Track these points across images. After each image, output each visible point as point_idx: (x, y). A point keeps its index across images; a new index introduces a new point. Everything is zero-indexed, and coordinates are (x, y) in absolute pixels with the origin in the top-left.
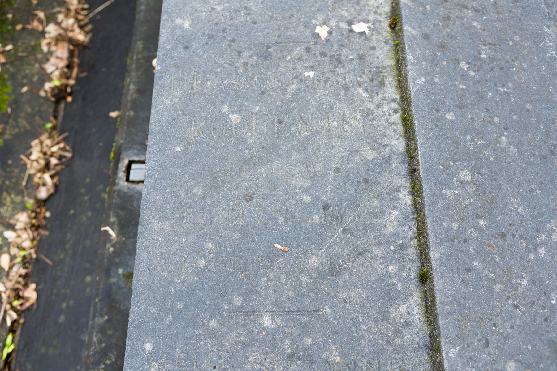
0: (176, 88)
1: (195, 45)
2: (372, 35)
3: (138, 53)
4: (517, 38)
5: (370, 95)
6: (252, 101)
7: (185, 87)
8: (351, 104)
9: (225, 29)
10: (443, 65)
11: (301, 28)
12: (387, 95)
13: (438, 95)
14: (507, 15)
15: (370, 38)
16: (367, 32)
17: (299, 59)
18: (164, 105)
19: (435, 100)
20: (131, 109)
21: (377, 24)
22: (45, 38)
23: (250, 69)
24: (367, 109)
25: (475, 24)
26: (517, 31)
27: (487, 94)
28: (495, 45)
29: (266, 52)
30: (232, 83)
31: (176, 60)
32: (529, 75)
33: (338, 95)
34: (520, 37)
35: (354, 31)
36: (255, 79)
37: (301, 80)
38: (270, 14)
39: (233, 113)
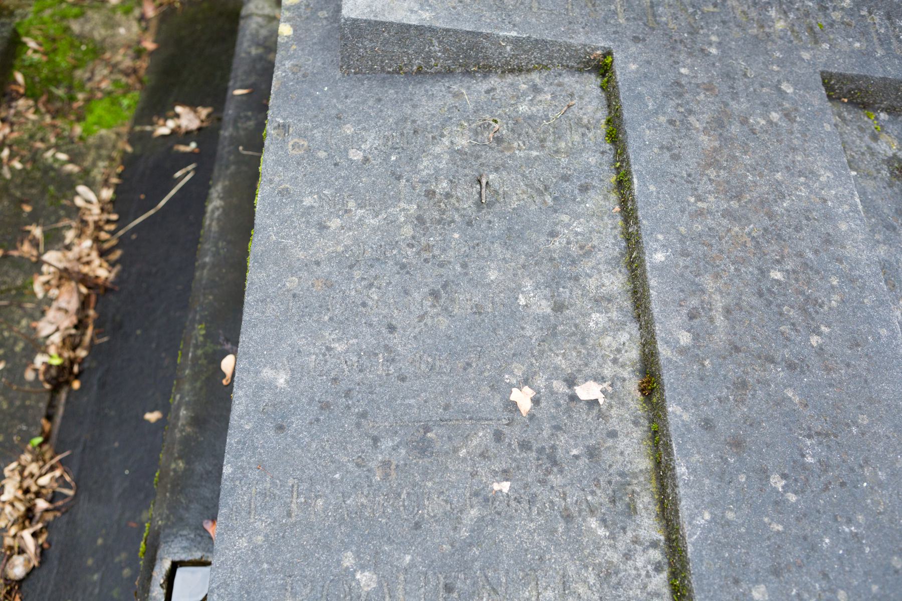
0: (259, 515)
1: (296, 423)
2: (610, 406)
3: (196, 347)
4: (863, 420)
5: (611, 533)
6: (397, 544)
7: (276, 511)
8: (577, 551)
9: (350, 390)
10: (740, 483)
11: (485, 390)
12: (642, 532)
13: (736, 548)
14: (843, 372)
15: (607, 414)
16: (601, 401)
17: (483, 455)
18: (236, 550)
19: (731, 559)
20: (180, 458)
21: (619, 384)
22: (41, 273)
23: (394, 475)
24: (607, 562)
25: (790, 393)
26: (863, 404)
27: (822, 541)
28: (827, 435)
29: (423, 439)
30: (362, 505)
31: (260, 454)
32: (891, 496)
33: (554, 531)
34: (869, 416)
35: (578, 398)
36: (404, 496)
37: (486, 500)
38: (430, 360)
39: (363, 568)
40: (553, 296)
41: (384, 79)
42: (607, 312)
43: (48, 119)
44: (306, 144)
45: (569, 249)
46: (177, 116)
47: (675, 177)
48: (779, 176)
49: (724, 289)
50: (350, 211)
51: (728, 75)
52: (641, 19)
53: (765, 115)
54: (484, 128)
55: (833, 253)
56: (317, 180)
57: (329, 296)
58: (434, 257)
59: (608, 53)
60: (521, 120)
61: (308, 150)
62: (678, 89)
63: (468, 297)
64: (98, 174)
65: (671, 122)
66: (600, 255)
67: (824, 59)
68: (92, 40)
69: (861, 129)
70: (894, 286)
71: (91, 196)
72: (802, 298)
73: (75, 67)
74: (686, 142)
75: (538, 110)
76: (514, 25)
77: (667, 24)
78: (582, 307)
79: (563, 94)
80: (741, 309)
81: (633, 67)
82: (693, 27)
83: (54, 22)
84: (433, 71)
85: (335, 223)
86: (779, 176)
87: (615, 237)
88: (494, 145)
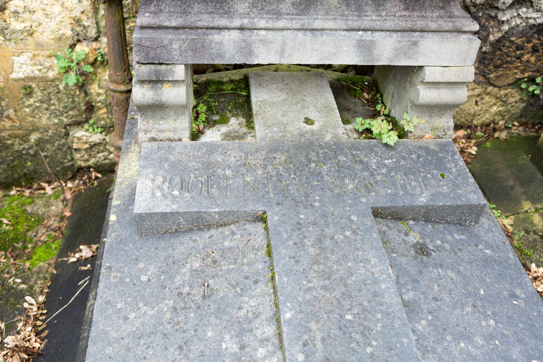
40: (239, 342)
41: (159, 237)
42: (266, 347)
43: (12, 261)
44: (120, 275)
45: (248, 315)
46: (81, 251)
47: (297, 271)
48: (350, 264)
49: (321, 328)
50: (140, 308)
51: (324, 216)
52: (281, 193)
53: (343, 234)
54: (208, 256)
55: (378, 301)
56: (125, 294)
57: (127, 355)
58: (181, 328)
59: (265, 213)
60: (225, 250)
61: (121, 279)
62: (299, 226)
63: (197, 347)
64: (37, 289)
65: (295, 244)
66: (263, 317)
67: (372, 201)
68: (38, 215)
69: (399, 231)
70: (418, 313)
71: (33, 301)
72: (362, 328)
73: (28, 231)
74: (302, 253)
75: (234, 244)
76: (218, 205)
77: (294, 194)
78: (254, 346)
79: (246, 234)
80: (330, 338)
81: (276, 218)
82: (307, 193)
83: (18, 208)
84: (183, 230)
85: (132, 316)
86: (350, 264)
87: (271, 306)
88: (212, 264)
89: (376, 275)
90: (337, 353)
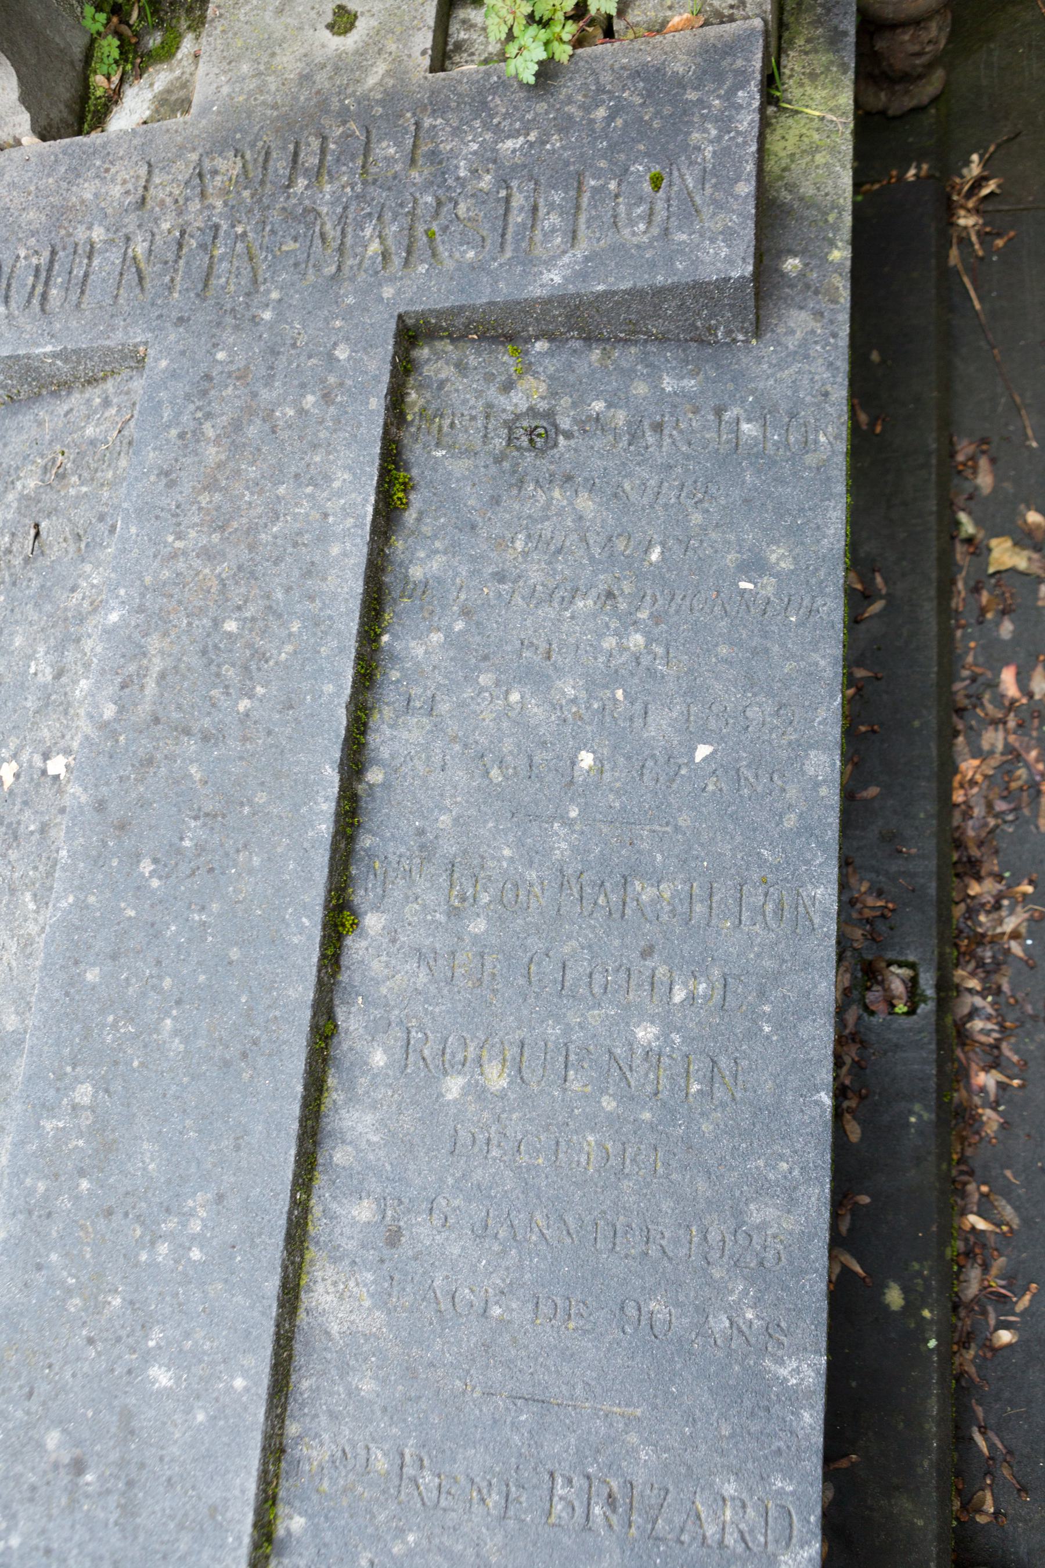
4: (261, 798)
65: (182, 436)
69: (489, 378)
89: (331, 519)
90: (179, 707)
